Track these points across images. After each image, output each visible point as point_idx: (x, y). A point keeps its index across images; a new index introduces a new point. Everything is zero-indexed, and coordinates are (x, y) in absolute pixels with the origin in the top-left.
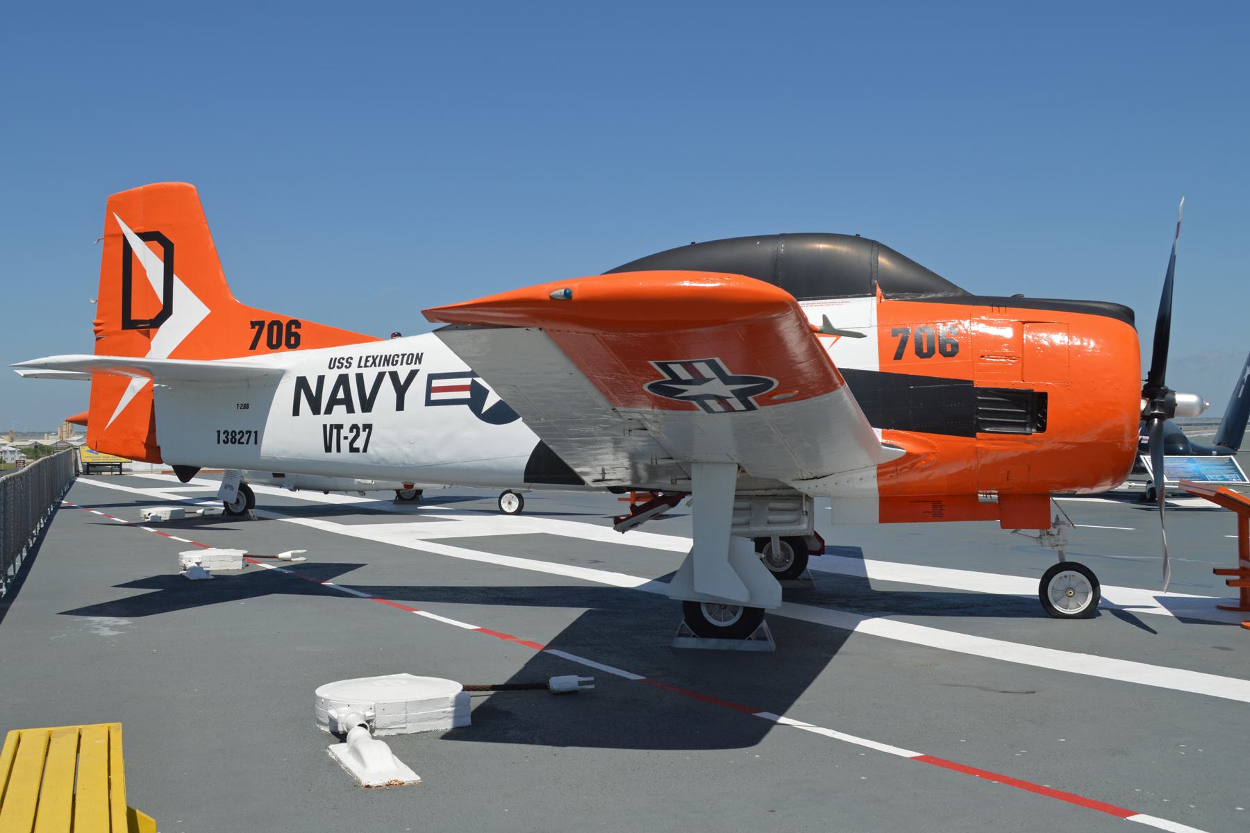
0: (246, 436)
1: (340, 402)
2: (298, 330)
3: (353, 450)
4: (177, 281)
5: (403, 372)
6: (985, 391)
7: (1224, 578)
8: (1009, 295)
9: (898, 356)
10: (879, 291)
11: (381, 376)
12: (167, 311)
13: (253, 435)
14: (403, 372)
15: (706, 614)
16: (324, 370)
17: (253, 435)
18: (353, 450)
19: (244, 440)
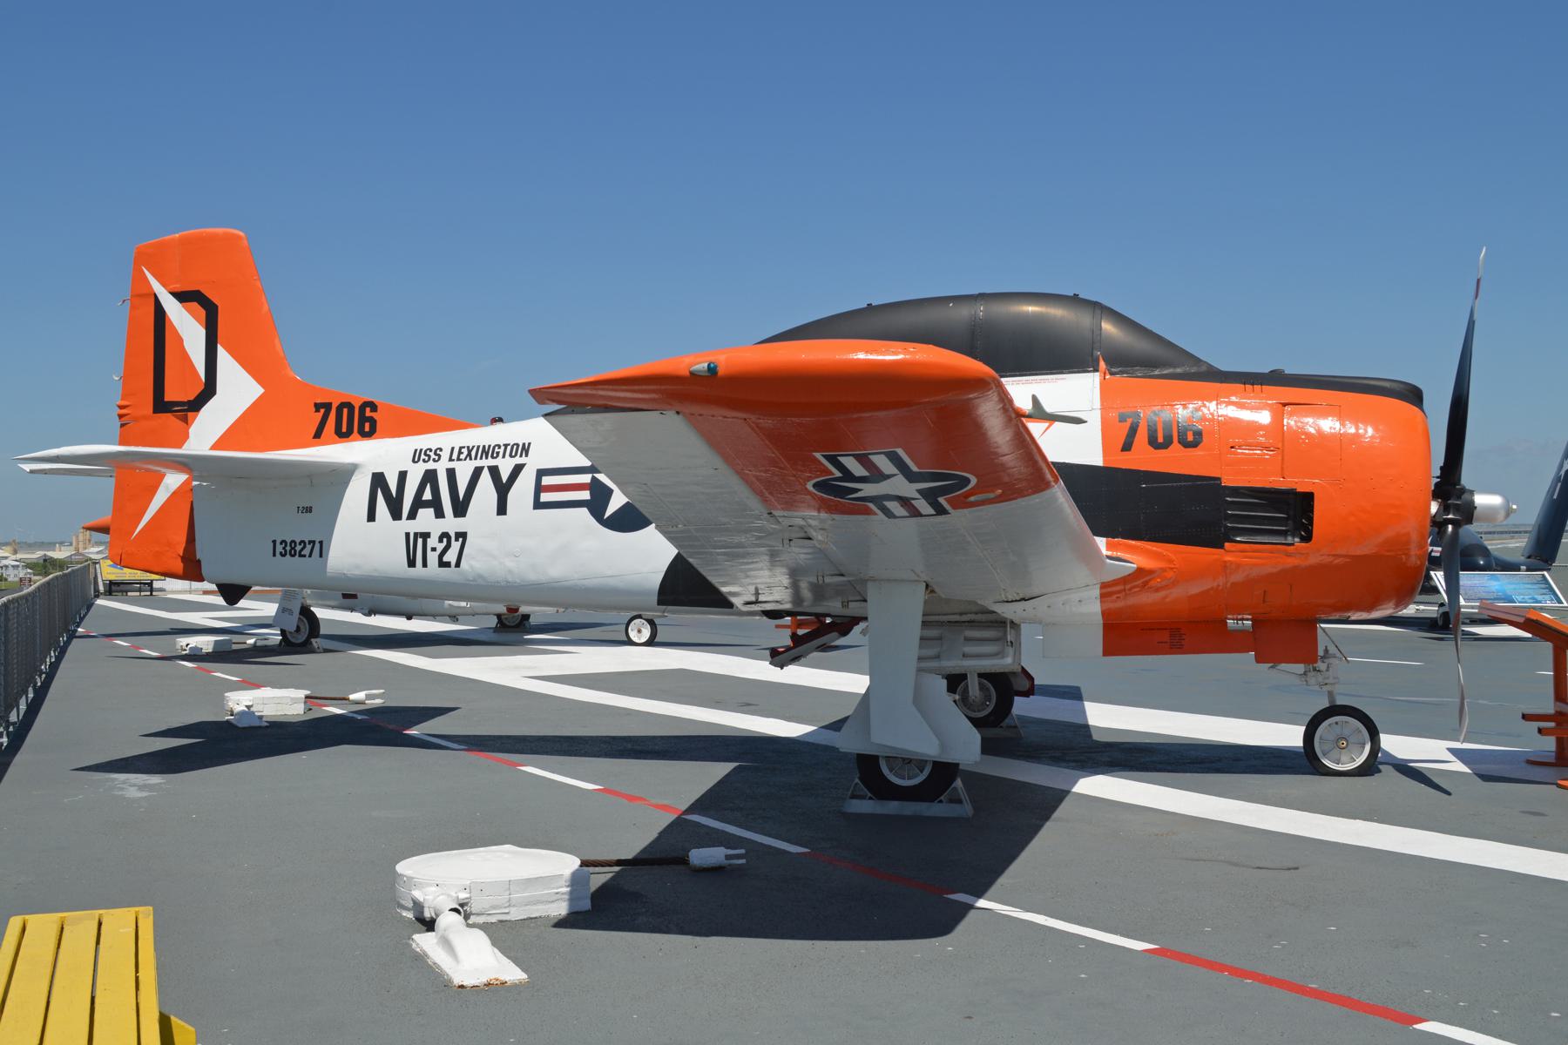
0: (309, 547)
1: (427, 504)
2: (373, 414)
3: (443, 564)
4: (222, 353)
5: (506, 466)
6: (1236, 491)
7: (1536, 725)
8: (1266, 370)
9: (1127, 447)
10: (1102, 364)
11: (477, 472)
12: (209, 390)
13: (317, 546)
14: (506, 466)
15: (885, 771)
16: (407, 465)
17: (317, 546)
18: (443, 564)
19: (306, 552)
